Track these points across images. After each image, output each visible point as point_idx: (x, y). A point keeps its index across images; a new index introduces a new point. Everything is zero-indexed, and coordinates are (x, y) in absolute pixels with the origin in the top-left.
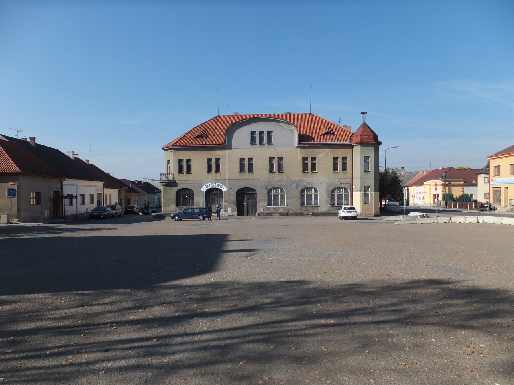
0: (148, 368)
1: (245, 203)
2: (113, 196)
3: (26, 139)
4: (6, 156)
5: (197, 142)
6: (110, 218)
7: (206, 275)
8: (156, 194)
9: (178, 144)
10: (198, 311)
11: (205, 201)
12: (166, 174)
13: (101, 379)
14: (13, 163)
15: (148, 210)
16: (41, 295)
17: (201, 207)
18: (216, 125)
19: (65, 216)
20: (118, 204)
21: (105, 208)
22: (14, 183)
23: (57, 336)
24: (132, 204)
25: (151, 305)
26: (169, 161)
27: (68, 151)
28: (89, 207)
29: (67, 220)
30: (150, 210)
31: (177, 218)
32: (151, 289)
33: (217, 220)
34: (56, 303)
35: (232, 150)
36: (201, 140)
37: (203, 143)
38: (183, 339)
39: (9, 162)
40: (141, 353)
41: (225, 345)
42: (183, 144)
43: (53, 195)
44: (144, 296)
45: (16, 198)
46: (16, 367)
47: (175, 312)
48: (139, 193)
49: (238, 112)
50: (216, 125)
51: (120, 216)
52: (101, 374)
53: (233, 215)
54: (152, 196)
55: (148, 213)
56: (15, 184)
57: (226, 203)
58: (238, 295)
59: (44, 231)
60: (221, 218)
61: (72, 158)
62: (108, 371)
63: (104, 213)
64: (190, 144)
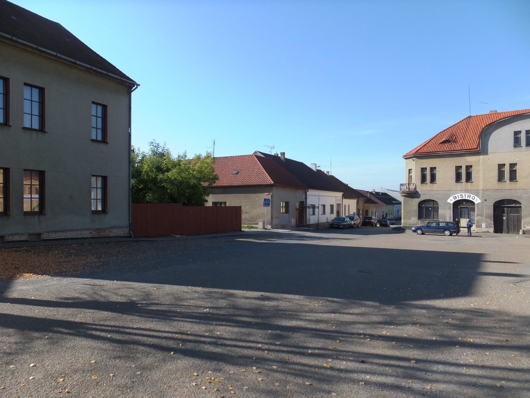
0: (409, 391)
1: (504, 218)
2: (351, 206)
3: (278, 154)
4: (262, 170)
5: (443, 148)
6: (348, 228)
7: (463, 299)
8: (395, 205)
9: (421, 151)
10: (460, 339)
11: (452, 214)
12: (407, 184)
13: (362, 390)
14: (268, 176)
15: (386, 222)
16: (297, 297)
17: (448, 220)
18: (467, 128)
19: (308, 225)
20: (356, 214)
21: (344, 219)
22: (269, 194)
23: (315, 337)
24: (370, 215)
25: (404, 323)
26: (410, 170)
27: (311, 164)
28: (330, 217)
29: (310, 229)
30: (388, 222)
31: (419, 232)
32: (400, 306)
33: (467, 236)
34: (311, 306)
35: (488, 155)
36: (448, 145)
37: (450, 149)
38: (446, 368)
39: (265, 175)
40: (399, 372)
41: (501, 386)
42: (426, 151)
43: (299, 205)
44: (394, 313)
45: (270, 207)
46: (286, 359)
47: (433, 335)
48: (377, 205)
49: (495, 110)
50: (467, 128)
51: (358, 227)
52: (361, 384)
53: (488, 232)
54: (390, 207)
55: (386, 225)
56: (269, 195)
57: (479, 217)
58: (509, 328)
59: (292, 238)
60: (472, 234)
61: (314, 170)
62: (367, 383)
63: (343, 224)
64: (435, 151)
